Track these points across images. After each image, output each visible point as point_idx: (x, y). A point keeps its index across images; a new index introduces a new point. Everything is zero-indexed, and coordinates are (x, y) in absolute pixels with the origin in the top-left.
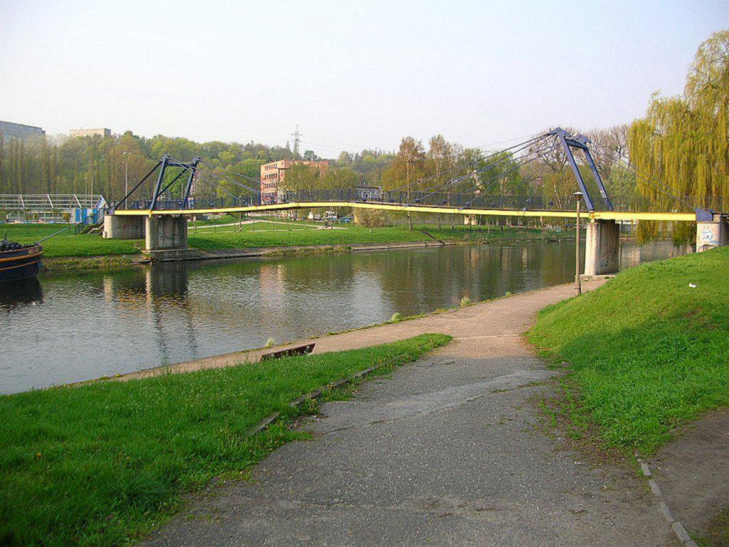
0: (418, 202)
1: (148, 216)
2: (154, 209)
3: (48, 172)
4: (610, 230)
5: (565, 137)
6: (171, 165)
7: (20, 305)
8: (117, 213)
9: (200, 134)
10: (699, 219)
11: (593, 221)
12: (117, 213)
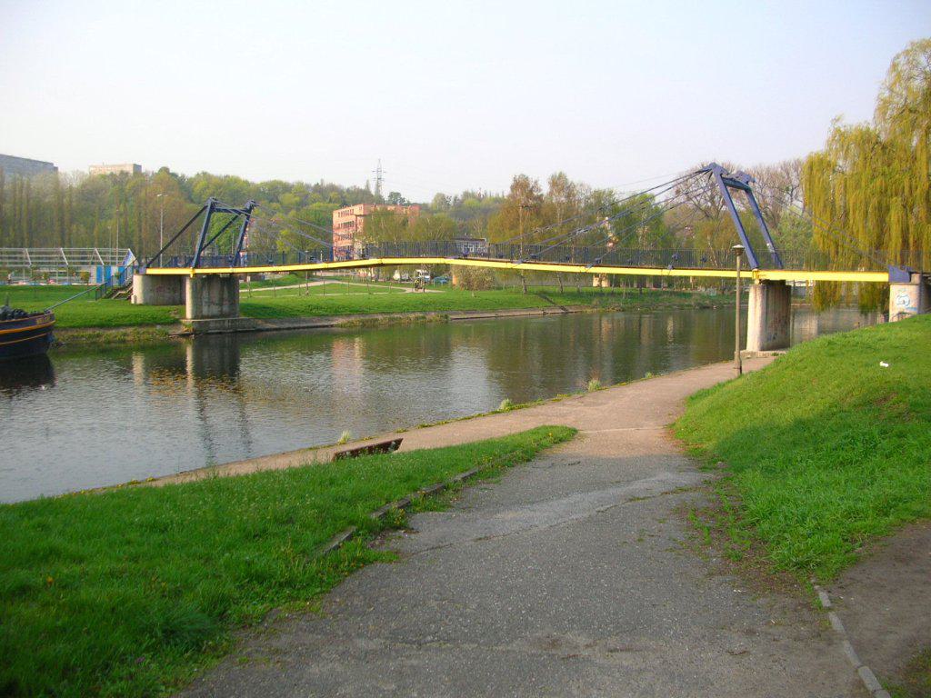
0: (534, 258)
1: (189, 275)
2: (197, 266)
3: (61, 220)
4: (779, 293)
5: (721, 175)
6: (219, 210)
7: (25, 389)
8: (150, 271)
9: (255, 170)
10: (893, 280)
11: (757, 282)
12: (150, 271)
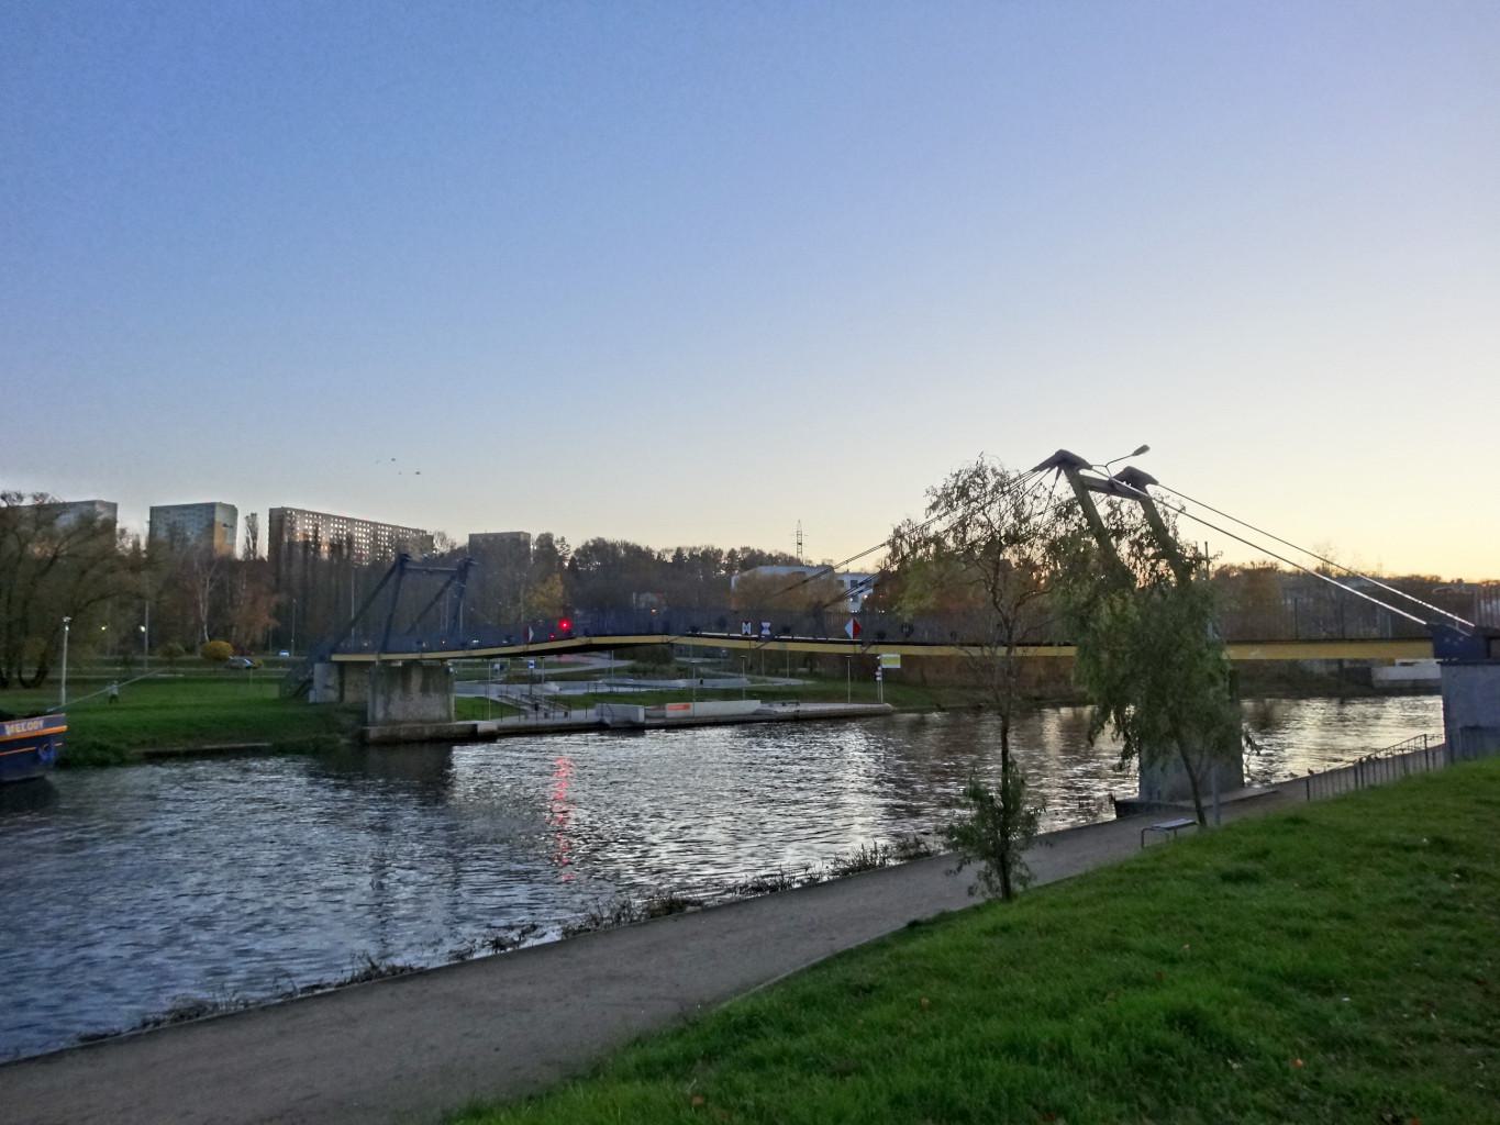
1: (374, 662)
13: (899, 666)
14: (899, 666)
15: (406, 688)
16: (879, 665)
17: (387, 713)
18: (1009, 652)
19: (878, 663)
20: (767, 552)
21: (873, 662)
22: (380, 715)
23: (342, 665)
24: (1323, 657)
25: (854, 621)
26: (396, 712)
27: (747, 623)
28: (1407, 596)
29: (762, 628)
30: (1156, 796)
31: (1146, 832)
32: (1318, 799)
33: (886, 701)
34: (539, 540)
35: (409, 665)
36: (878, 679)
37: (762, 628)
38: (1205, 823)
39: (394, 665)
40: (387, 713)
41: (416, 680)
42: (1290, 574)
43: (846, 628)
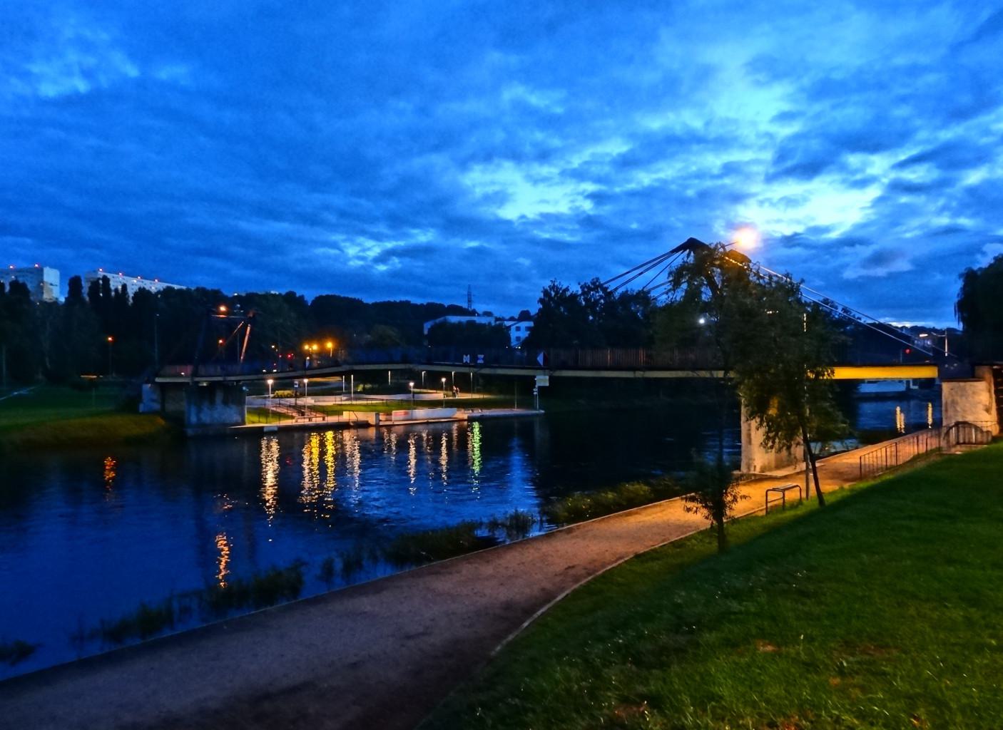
1: (188, 383)
13: (547, 384)
14: (547, 384)
15: (212, 402)
16: (535, 384)
17: (199, 419)
18: (725, 374)
19: (535, 382)
20: (305, 299)
21: (531, 381)
22: (194, 419)
23: (162, 385)
24: (400, 398)
25: (544, 354)
26: (206, 418)
27: (467, 355)
28: (248, 332)
29: (478, 359)
30: (752, 469)
31: (769, 492)
32: (894, 463)
33: (540, 408)
34: (136, 294)
35: (212, 384)
36: (535, 393)
37: (478, 359)
38: (832, 478)
39: (201, 385)
40: (199, 419)
41: (219, 397)
42: (963, 323)
43: (538, 359)
